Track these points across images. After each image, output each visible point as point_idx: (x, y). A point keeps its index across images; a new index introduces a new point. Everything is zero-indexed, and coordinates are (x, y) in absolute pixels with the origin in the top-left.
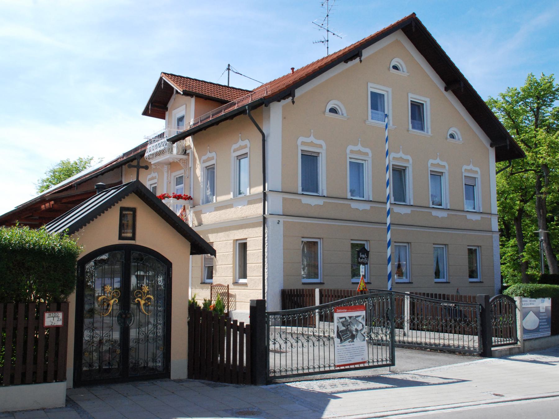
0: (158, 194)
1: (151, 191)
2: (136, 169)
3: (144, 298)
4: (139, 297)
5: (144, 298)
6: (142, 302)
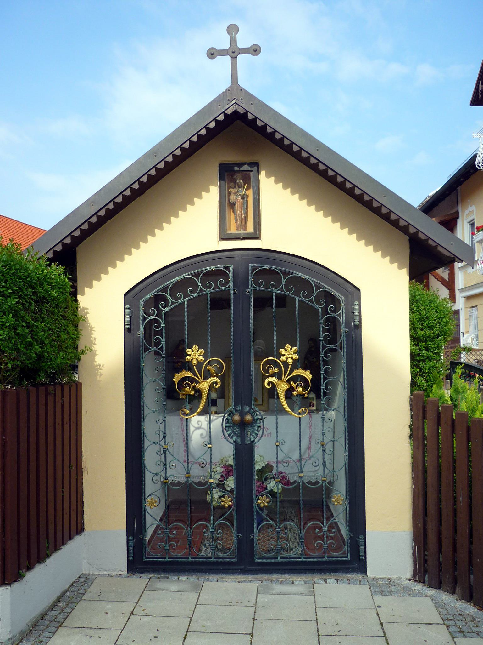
0: (92, 336)
1: (471, 246)
2: (228, 58)
3: (285, 378)
4: (273, 375)
5: (285, 378)
6: (282, 387)
